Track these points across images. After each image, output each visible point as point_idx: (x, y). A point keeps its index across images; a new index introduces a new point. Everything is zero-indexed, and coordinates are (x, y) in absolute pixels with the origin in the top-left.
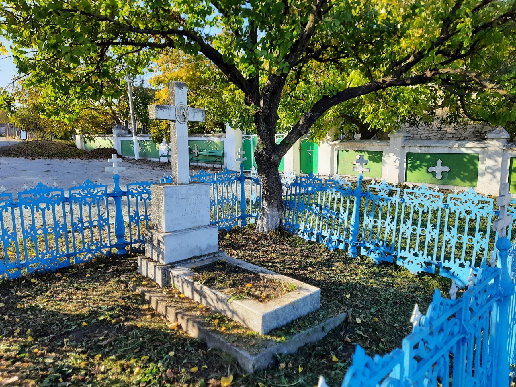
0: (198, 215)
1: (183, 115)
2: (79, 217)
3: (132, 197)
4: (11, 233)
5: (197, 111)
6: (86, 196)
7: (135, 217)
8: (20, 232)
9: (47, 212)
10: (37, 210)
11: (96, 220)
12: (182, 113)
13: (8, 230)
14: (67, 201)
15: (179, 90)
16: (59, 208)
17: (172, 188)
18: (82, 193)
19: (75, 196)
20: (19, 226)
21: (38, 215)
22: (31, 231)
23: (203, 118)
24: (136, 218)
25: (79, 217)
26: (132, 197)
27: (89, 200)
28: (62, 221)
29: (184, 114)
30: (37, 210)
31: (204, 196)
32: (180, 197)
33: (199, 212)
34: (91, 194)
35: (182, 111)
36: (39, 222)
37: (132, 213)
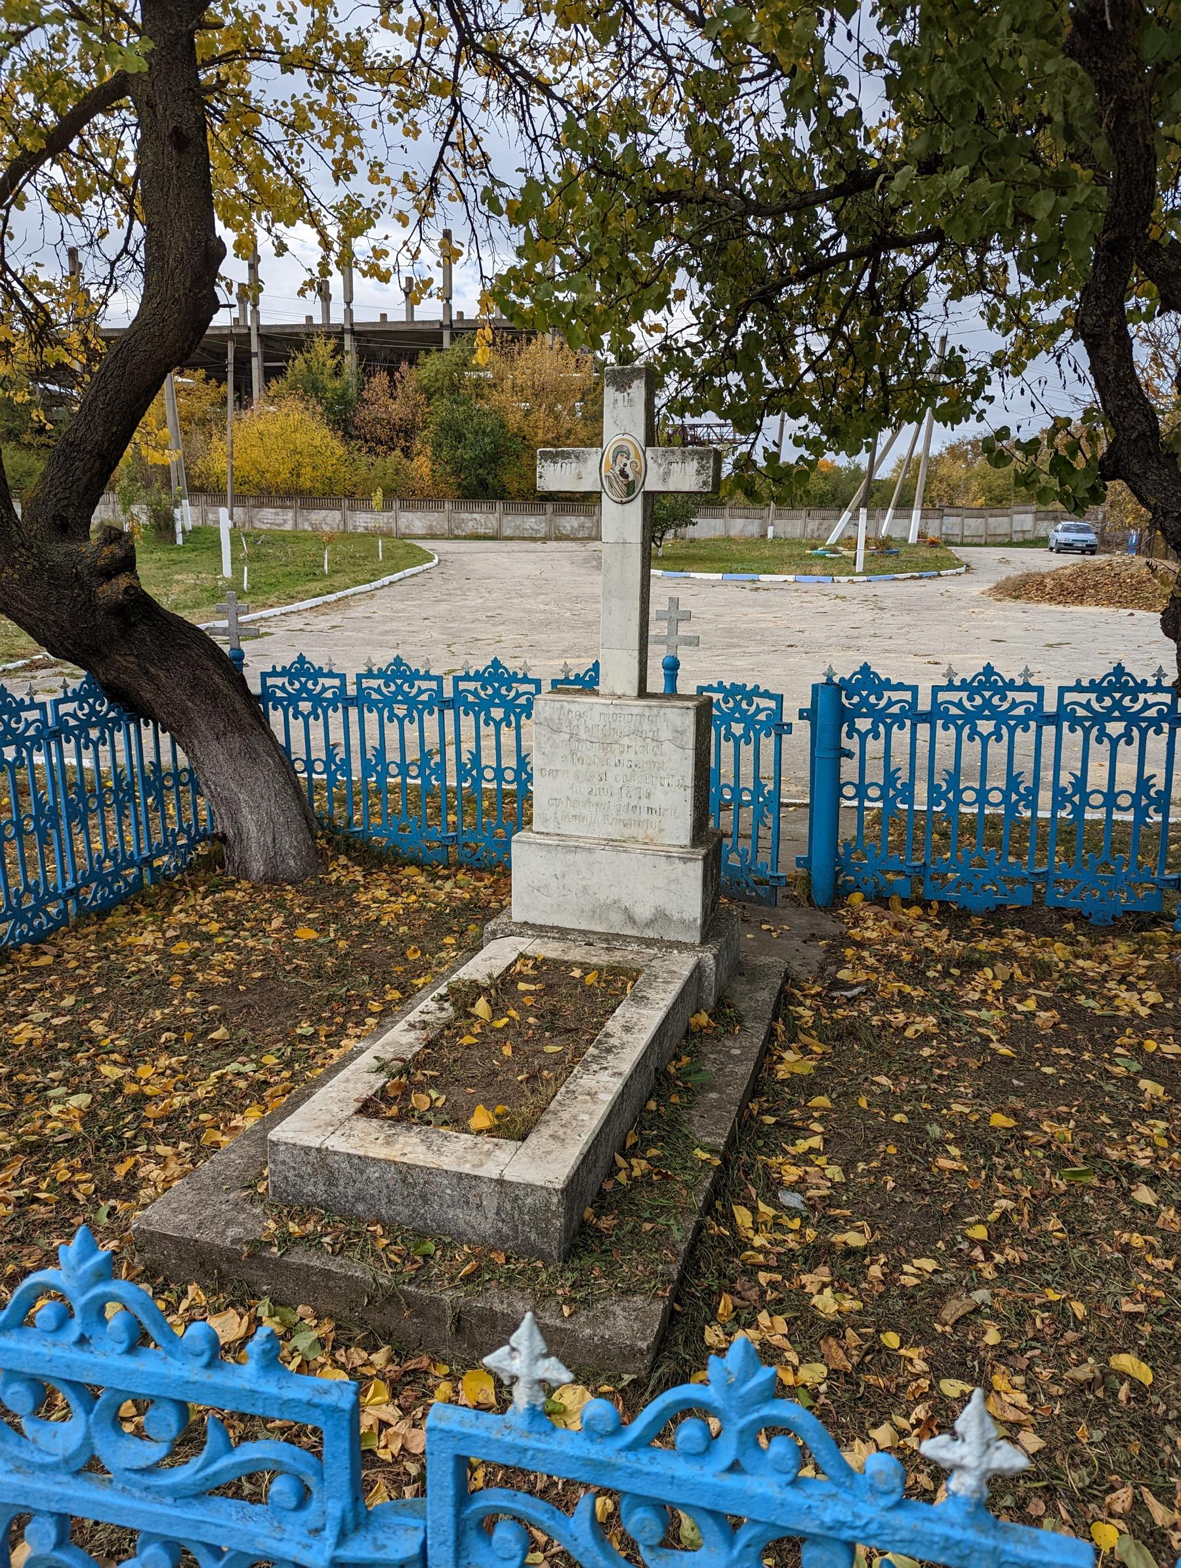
0: (645, 803)
1: (623, 473)
2: (1078, 773)
3: (1072, 730)
4: (1026, 789)
5: (678, 457)
6: (978, 714)
7: (376, 765)
8: (451, 767)
9: (504, 729)
10: (971, 738)
11: (876, 784)
12: (617, 469)
13: (899, 774)
14: (352, 705)
15: (619, 395)
16: (431, 722)
17: (558, 705)
18: (967, 704)
19: (1074, 710)
20: (1047, 776)
21: (1099, 752)
22: (1073, 795)
23: (703, 478)
24: (892, 793)
25: (1078, 773)
26: (946, 728)
27: (305, 706)
28: (904, 776)
29: (628, 470)
30: (1099, 740)
31: (667, 746)
32: (583, 736)
33: (648, 796)
34: (309, 691)
35: (622, 460)
36: (1097, 777)
37: (465, 757)
